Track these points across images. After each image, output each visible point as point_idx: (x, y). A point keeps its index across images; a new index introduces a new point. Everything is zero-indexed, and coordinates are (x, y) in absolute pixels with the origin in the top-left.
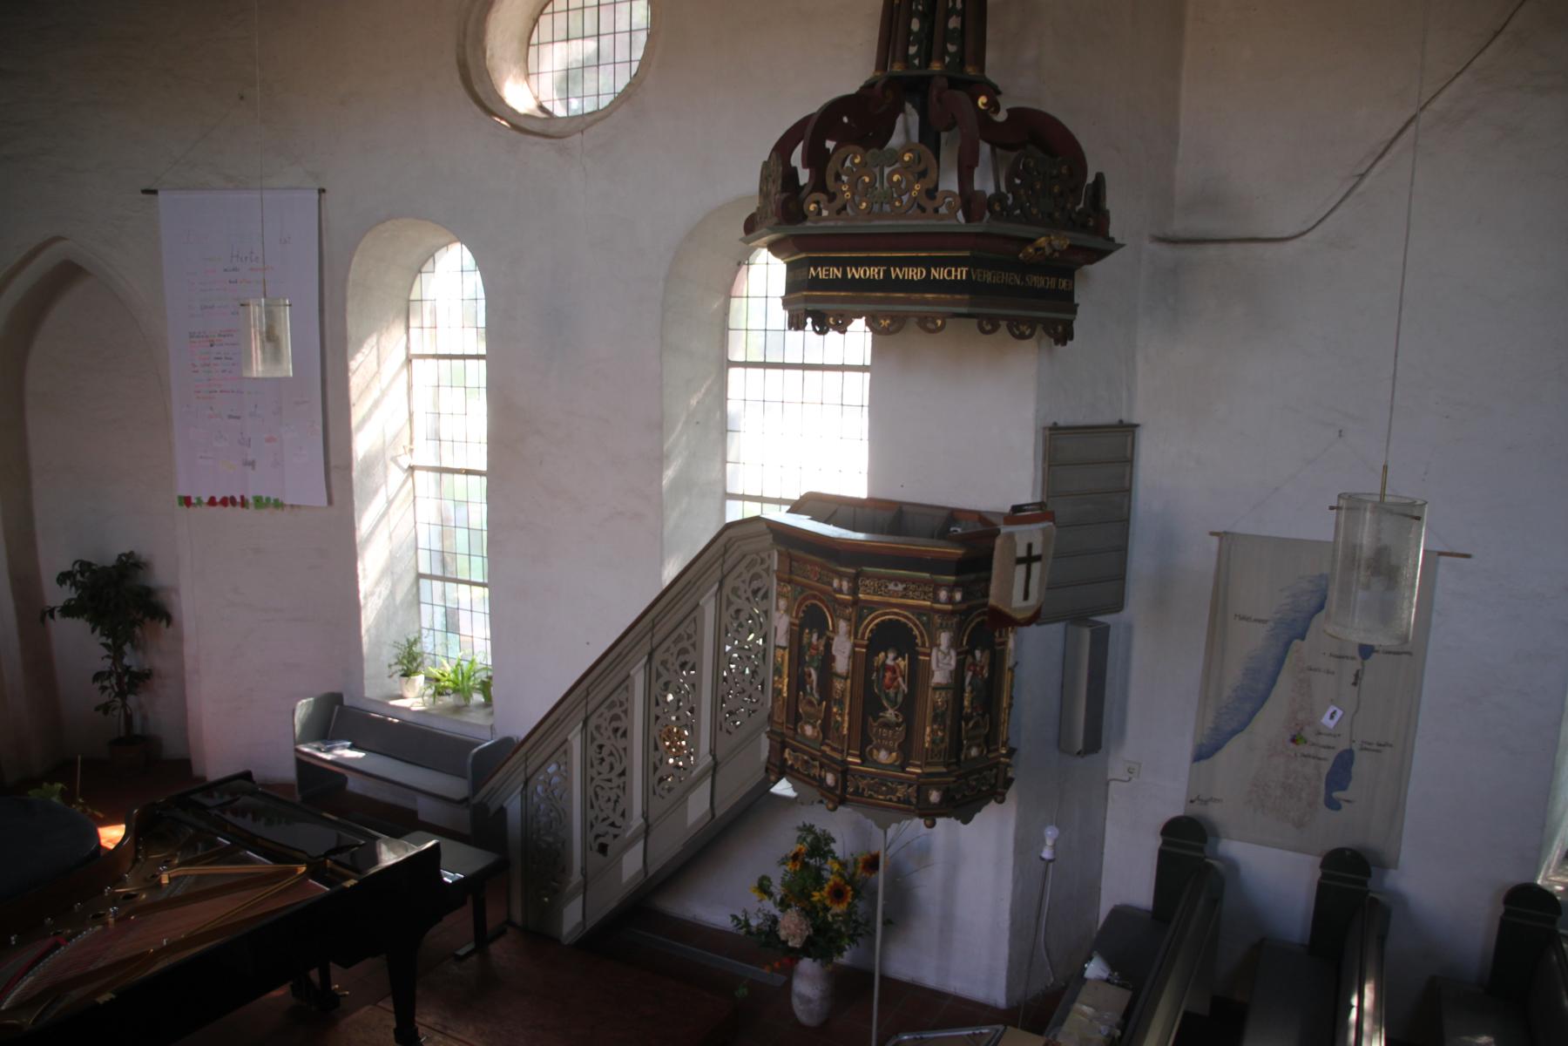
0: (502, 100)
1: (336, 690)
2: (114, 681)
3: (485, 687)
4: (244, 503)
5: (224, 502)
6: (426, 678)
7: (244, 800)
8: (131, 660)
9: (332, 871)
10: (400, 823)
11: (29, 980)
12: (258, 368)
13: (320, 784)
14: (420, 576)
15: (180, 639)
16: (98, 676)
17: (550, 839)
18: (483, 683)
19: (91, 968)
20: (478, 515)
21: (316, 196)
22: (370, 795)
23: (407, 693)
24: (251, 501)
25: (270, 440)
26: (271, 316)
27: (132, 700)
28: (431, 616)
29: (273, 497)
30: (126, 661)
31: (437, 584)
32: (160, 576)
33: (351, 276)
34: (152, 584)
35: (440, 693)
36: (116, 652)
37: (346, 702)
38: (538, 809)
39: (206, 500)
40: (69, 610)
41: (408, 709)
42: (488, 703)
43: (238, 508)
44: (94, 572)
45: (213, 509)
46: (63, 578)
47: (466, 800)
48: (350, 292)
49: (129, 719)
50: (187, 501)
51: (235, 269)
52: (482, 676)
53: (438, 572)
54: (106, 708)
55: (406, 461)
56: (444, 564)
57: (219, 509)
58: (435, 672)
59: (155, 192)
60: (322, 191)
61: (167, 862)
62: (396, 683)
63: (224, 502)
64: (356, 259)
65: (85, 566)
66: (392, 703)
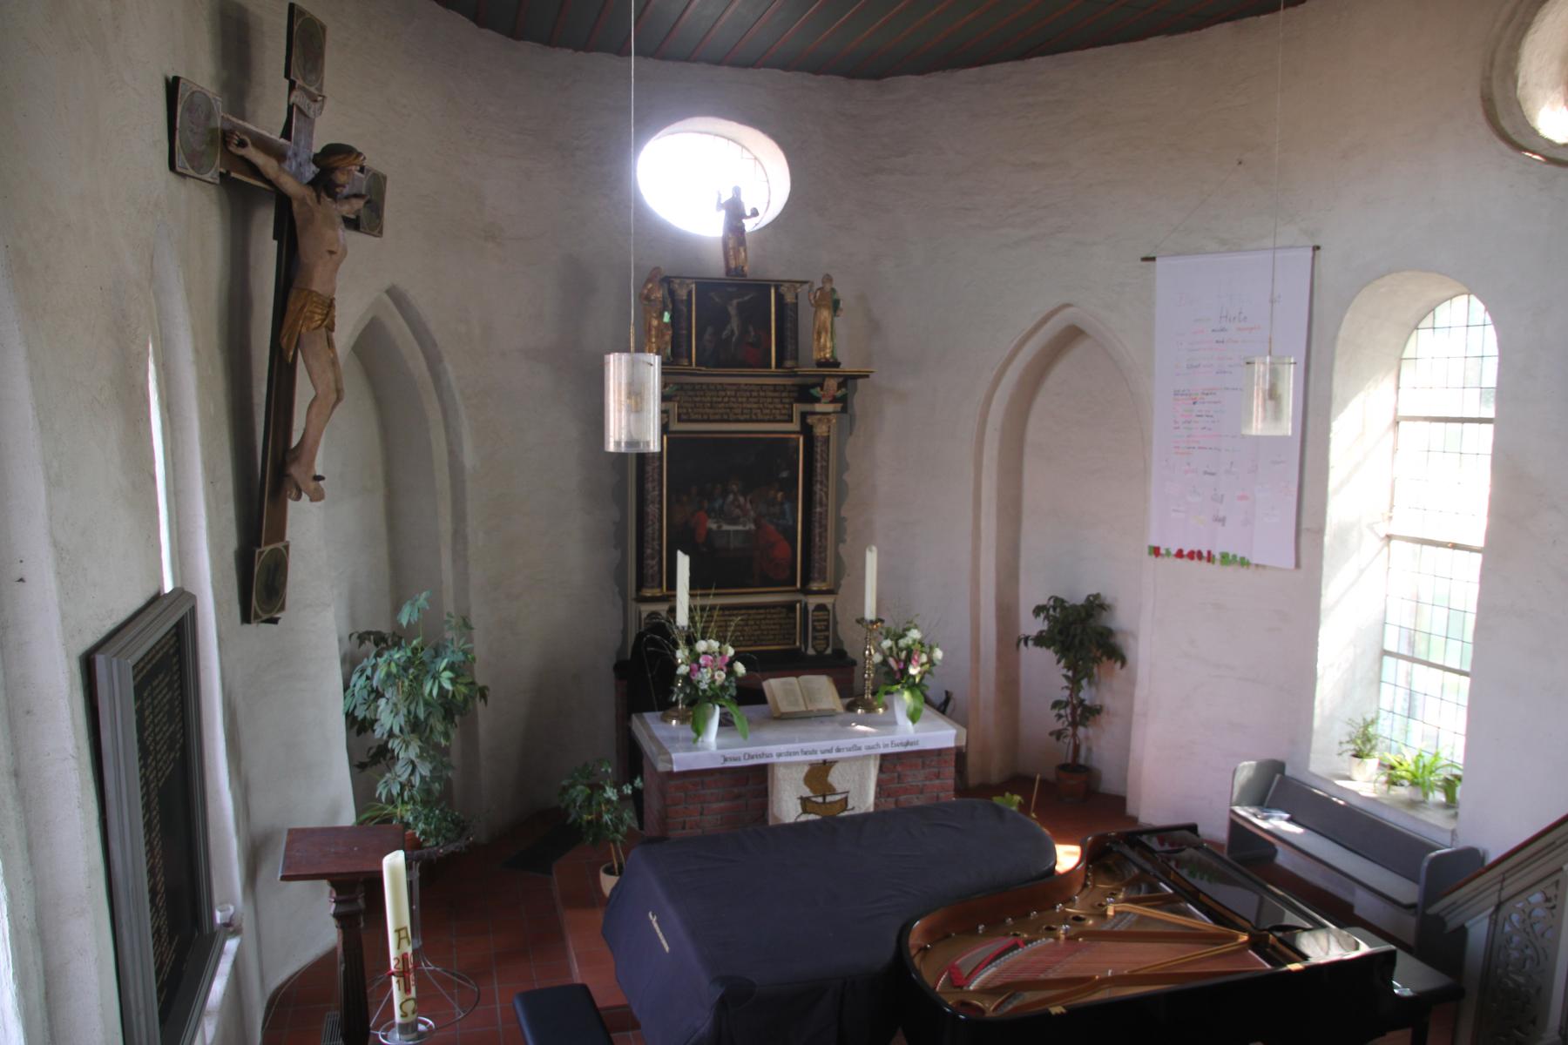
0: (1535, 132)
1: (1279, 757)
2: (1069, 710)
3: (1449, 786)
4: (1210, 558)
5: (1191, 555)
6: (1381, 765)
7: (1189, 852)
8: (1086, 694)
9: (1273, 947)
10: (1343, 916)
11: (991, 970)
12: (1258, 426)
13: (1250, 851)
14: (1386, 653)
15: (1132, 682)
16: (1056, 705)
17: (1521, 980)
18: (1447, 780)
19: (1042, 976)
20: (1467, 594)
21: (1310, 254)
22: (1300, 873)
23: (1355, 775)
24: (1218, 557)
25: (1243, 498)
26: (1274, 373)
27: (1081, 730)
28: (1391, 697)
29: (1239, 555)
30: (1082, 695)
31: (1403, 664)
32: (1120, 620)
33: (1343, 333)
34: (1113, 625)
35: (1392, 782)
36: (1075, 683)
37: (1288, 772)
38: (1509, 940)
39: (1174, 551)
40: (1040, 640)
41: (1356, 794)
42: (1451, 803)
43: (1204, 563)
44: (1064, 608)
45: (1179, 561)
46: (1038, 610)
47: (1412, 906)
48: (1339, 349)
49: (1077, 748)
50: (1156, 551)
51: (1223, 330)
52: (1444, 773)
53: (1404, 651)
54: (1058, 734)
55: (1384, 529)
56: (1412, 644)
57: (1185, 562)
58: (1392, 759)
59: (1153, 259)
60: (1316, 248)
61: (1112, 895)
62: (1346, 763)
63: (1191, 555)
64: (1348, 316)
65: (1059, 602)
66: (1339, 783)
